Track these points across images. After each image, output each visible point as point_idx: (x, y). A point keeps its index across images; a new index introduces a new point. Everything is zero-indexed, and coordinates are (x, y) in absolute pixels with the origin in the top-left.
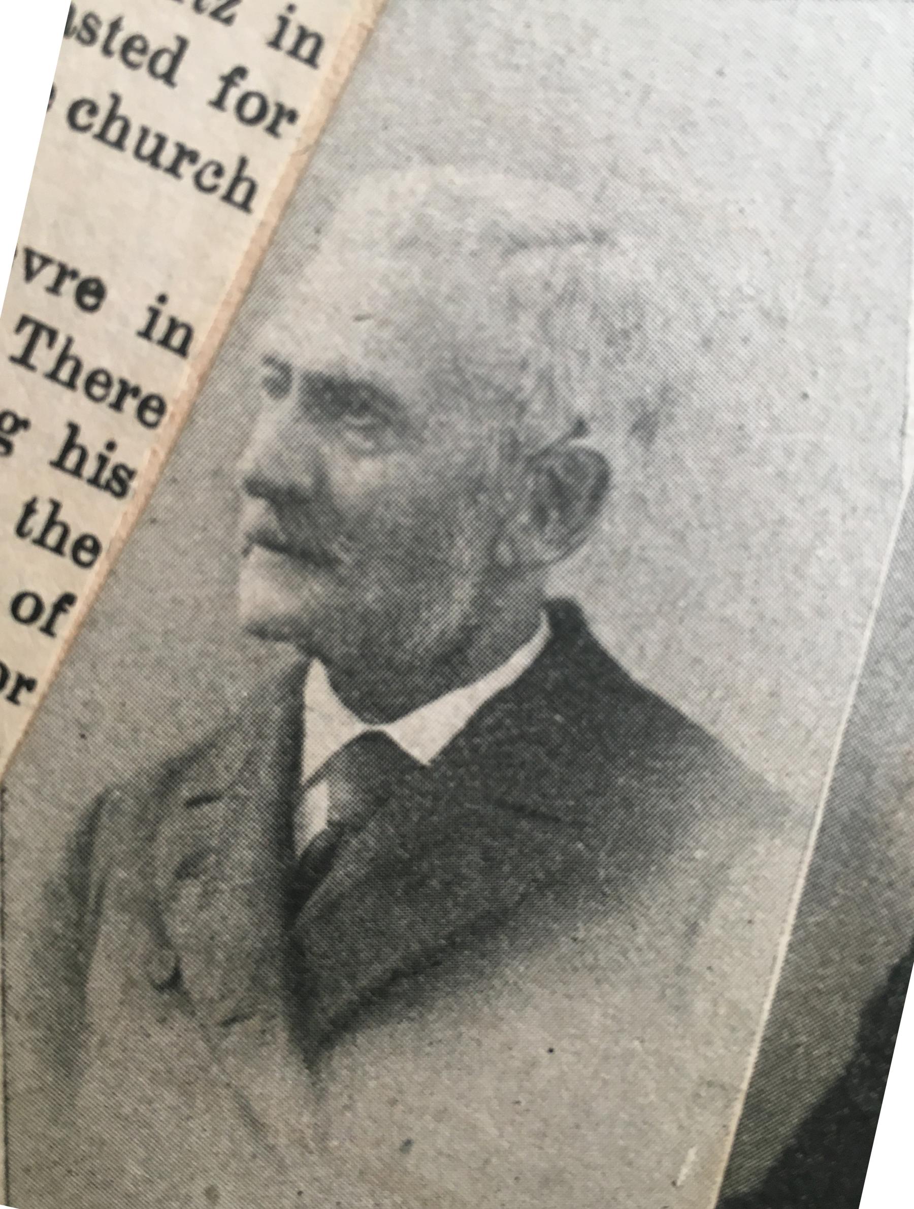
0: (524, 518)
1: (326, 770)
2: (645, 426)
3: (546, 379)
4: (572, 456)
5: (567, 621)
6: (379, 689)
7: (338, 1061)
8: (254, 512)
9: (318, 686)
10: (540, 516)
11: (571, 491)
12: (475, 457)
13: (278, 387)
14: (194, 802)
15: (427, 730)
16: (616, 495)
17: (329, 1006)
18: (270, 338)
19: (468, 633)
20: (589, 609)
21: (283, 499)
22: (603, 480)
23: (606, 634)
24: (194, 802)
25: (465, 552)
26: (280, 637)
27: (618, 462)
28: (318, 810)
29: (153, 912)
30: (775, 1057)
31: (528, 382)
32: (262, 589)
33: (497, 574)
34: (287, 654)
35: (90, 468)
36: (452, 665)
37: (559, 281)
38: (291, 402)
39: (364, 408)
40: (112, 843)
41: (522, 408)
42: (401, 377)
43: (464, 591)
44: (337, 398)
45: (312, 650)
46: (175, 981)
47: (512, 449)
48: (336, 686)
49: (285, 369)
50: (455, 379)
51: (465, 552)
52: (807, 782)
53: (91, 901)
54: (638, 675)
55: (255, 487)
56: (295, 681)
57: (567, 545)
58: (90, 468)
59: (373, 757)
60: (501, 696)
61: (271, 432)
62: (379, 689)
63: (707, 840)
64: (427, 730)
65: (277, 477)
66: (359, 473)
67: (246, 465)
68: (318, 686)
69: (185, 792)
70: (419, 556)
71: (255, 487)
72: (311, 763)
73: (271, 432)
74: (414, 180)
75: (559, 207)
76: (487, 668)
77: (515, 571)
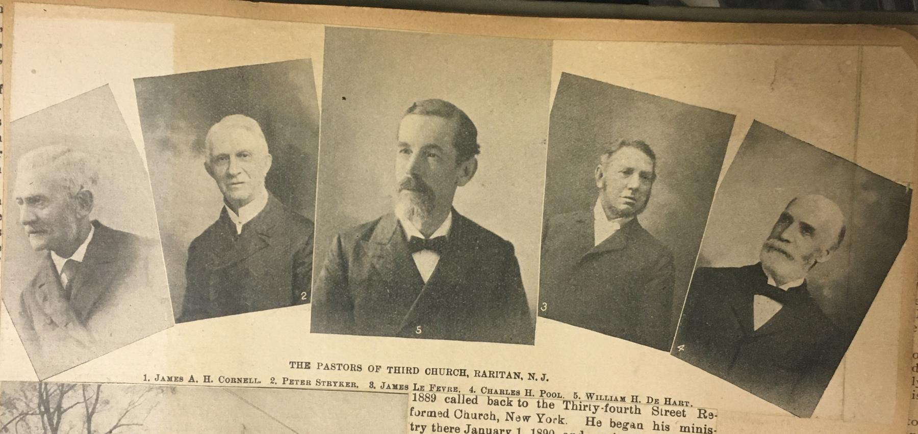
0: (79, 208)
1: (62, 272)
2: (94, 181)
3: (71, 180)
4: (83, 194)
5: (96, 224)
6: (66, 251)
7: (92, 323)
8: (27, 228)
9: (54, 256)
10: (83, 207)
11: (86, 200)
12: (65, 200)
13: (21, 203)
14: (40, 287)
15: (79, 255)
16: (95, 196)
17: (84, 314)
18: (16, 195)
19: (79, 233)
20: (100, 220)
21: (31, 223)
22: (91, 195)
23: (105, 222)
24: (40, 287)
25: (71, 219)
26: (42, 249)
27: (92, 191)
28: (65, 278)
29: (41, 309)
30: (173, 287)
31: (68, 183)
32: (35, 241)
33: (79, 221)
34: (46, 252)
35: (660, 428)
36: (79, 241)
37: (65, 162)
38: (25, 205)
39: (38, 201)
40: (29, 301)
41: (69, 188)
42: (43, 191)
43: (74, 226)
44: (33, 200)
45: (50, 249)
46: (52, 322)
47: (71, 197)
48: (57, 254)
49: (21, 199)
50: (54, 186)
51: (71, 219)
52: (155, 234)
53: (55, 422)
54: (114, 228)
55: (25, 223)
56: (49, 256)
57: (90, 210)
58: (660, 428)
59: (70, 265)
60: (90, 243)
61: (24, 213)
62: (66, 251)
63: (143, 251)
64: (79, 255)
65: (29, 220)
66: (44, 213)
67: (22, 219)
68: (54, 256)
69: (38, 285)
70: (62, 222)
71: (25, 223)
72: (59, 269)
73: (24, 213)
74: (31, 154)
75: (60, 148)
76: (85, 239)
77: (83, 217)
